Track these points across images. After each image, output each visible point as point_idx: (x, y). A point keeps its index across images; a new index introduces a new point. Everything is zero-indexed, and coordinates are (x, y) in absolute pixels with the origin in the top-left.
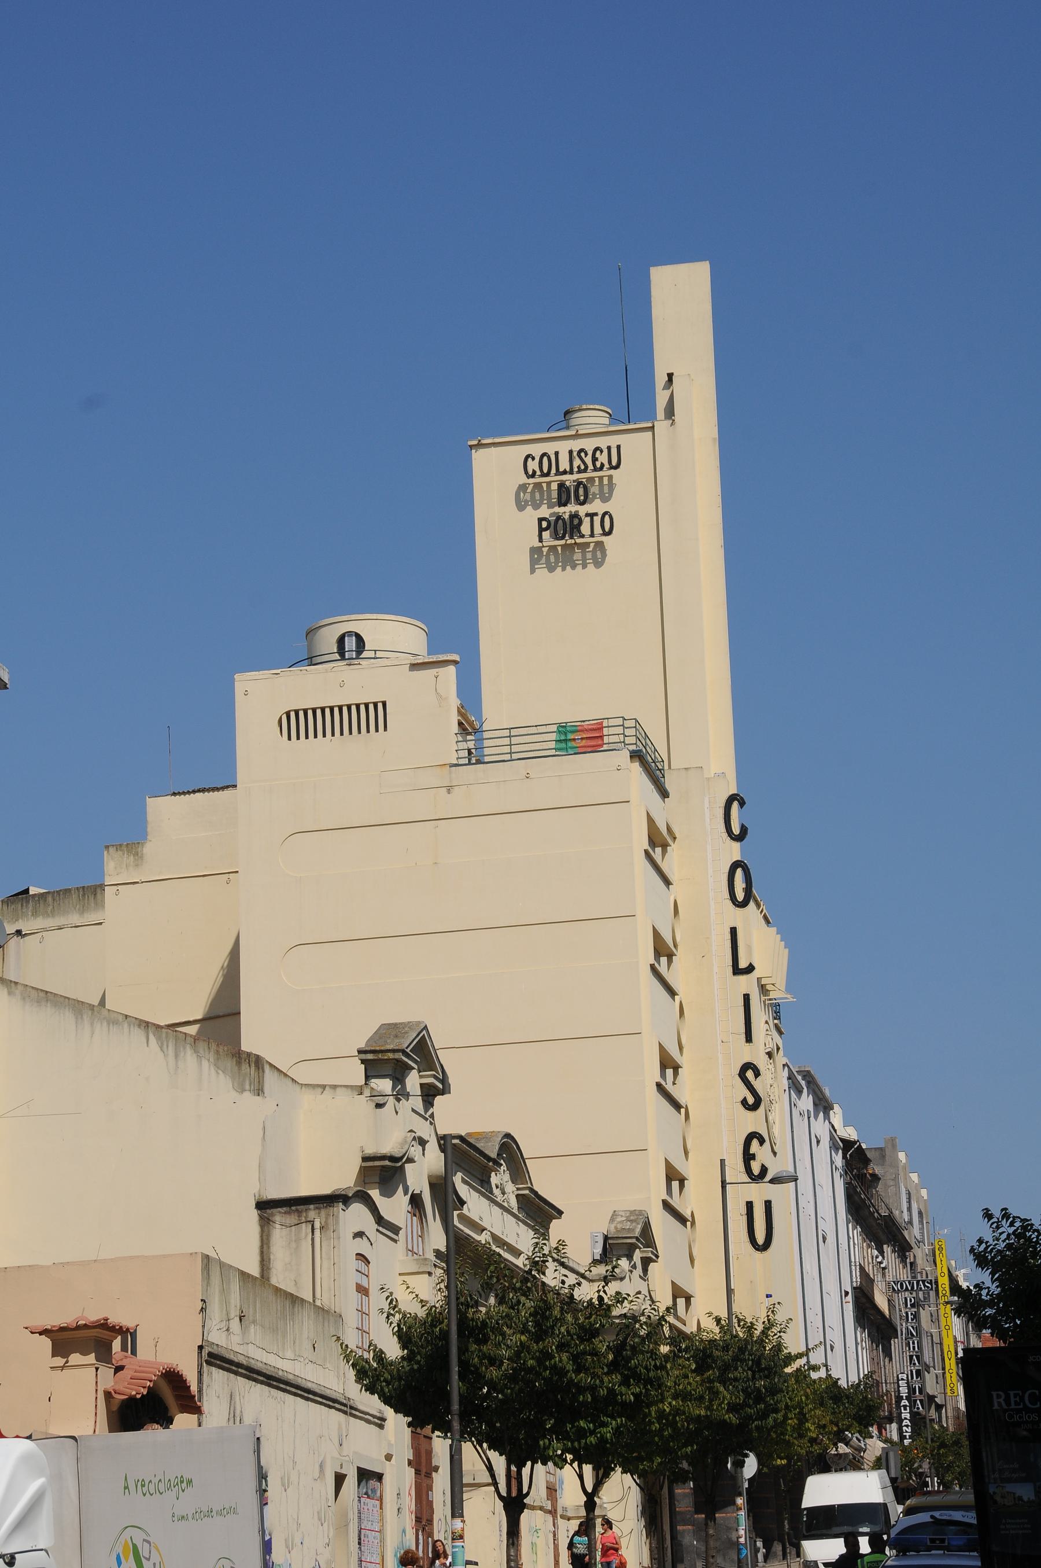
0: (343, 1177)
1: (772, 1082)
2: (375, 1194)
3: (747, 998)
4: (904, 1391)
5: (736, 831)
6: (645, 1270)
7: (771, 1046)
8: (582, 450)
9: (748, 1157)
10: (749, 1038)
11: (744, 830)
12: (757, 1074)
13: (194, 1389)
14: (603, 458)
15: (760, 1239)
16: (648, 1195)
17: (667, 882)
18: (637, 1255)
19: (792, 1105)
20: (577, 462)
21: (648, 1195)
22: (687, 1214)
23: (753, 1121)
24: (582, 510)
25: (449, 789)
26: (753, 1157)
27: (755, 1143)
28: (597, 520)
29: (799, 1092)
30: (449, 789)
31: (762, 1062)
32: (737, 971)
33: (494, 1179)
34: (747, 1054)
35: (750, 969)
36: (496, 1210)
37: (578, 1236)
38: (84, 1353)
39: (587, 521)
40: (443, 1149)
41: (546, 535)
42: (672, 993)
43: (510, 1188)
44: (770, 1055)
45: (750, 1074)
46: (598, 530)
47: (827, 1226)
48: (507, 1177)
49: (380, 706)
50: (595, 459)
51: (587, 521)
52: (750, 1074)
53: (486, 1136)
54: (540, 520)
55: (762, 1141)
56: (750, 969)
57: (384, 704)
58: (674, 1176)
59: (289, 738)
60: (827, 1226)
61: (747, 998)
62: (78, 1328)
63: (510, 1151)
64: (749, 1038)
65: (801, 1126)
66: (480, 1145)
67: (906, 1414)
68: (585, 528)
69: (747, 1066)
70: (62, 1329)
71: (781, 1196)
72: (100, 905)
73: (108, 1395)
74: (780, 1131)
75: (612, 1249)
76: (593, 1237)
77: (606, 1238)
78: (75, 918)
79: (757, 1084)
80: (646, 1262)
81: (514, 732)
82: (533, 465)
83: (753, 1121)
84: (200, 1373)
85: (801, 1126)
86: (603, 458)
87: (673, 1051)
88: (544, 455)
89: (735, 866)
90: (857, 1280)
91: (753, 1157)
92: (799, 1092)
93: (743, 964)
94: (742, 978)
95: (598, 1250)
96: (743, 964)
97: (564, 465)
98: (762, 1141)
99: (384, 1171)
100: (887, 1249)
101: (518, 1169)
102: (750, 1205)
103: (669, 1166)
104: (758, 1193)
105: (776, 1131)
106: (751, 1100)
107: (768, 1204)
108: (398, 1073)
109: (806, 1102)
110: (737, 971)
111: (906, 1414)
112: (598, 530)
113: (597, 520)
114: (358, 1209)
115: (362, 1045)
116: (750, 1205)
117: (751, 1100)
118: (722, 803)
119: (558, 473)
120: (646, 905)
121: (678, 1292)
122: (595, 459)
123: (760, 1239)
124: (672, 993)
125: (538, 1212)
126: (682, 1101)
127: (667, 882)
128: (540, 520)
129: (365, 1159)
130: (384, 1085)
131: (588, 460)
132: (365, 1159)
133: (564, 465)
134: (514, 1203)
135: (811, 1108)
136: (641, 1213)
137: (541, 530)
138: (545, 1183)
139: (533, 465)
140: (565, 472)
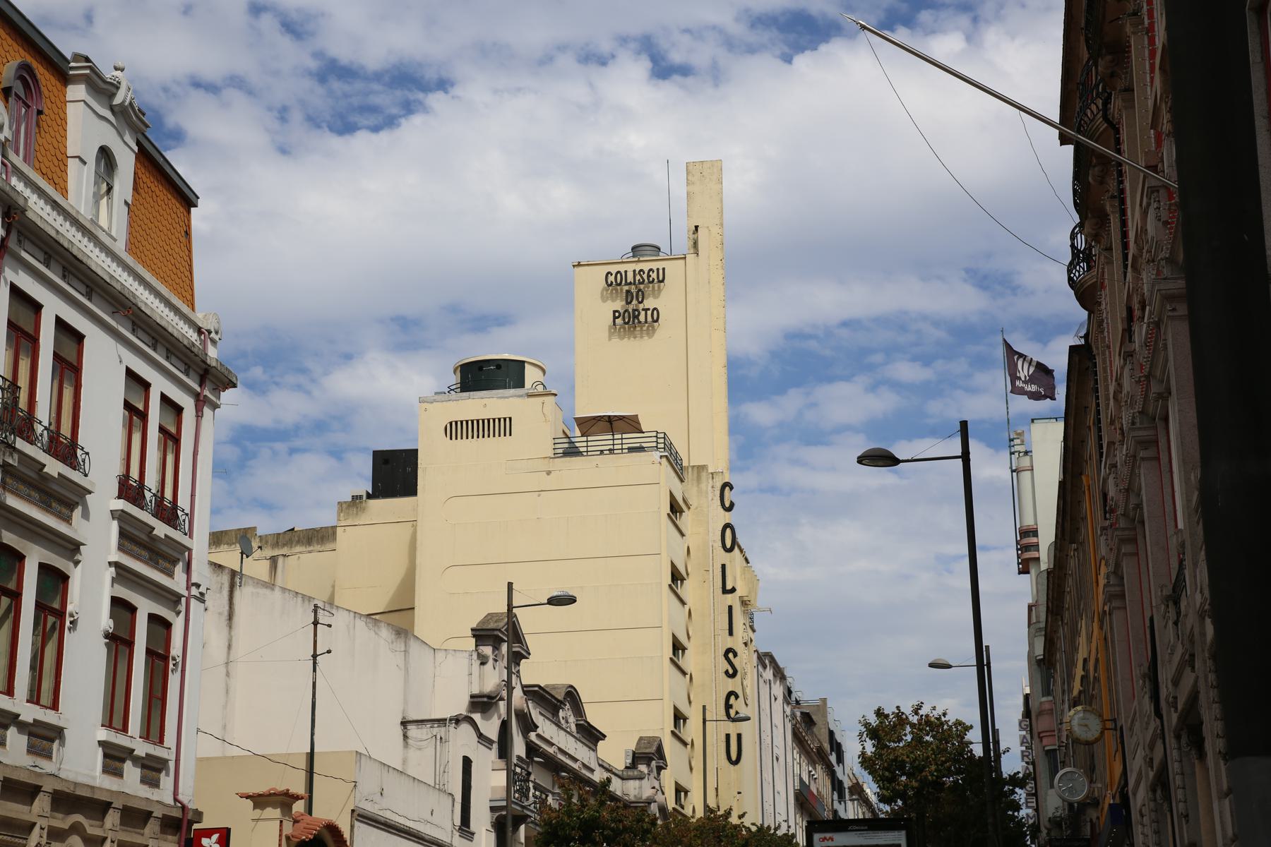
0: (460, 706)
1: (746, 660)
2: (477, 717)
3: (730, 608)
5: (727, 505)
6: (659, 774)
7: (746, 639)
9: (728, 707)
10: (731, 633)
11: (732, 505)
12: (735, 655)
13: (347, 835)
14: (654, 275)
15: (734, 757)
16: (661, 727)
17: (682, 535)
18: (654, 763)
19: (759, 675)
20: (638, 277)
21: (661, 727)
22: (689, 741)
23: (732, 685)
25: (549, 473)
26: (731, 706)
27: (733, 698)
28: (649, 313)
29: (765, 667)
30: (549, 473)
31: (740, 648)
32: (725, 591)
33: (561, 714)
34: (729, 643)
35: (733, 590)
36: (562, 733)
37: (615, 752)
38: (275, 808)
39: (643, 313)
40: (525, 693)
42: (683, 603)
43: (572, 719)
44: (746, 644)
45: (731, 655)
46: (649, 319)
47: (779, 751)
48: (570, 713)
50: (649, 276)
51: (643, 313)
52: (731, 655)
53: (554, 687)
54: (615, 312)
55: (737, 697)
56: (733, 590)
58: (679, 717)
60: (779, 751)
61: (730, 608)
62: (270, 795)
63: (572, 696)
64: (731, 633)
65: (765, 690)
66: (553, 693)
68: (642, 318)
69: (729, 650)
70: (260, 795)
71: (743, 727)
72: (334, 539)
73: (288, 838)
74: (751, 691)
75: (638, 758)
76: (627, 752)
77: (634, 753)
78: (318, 547)
79: (736, 662)
80: (659, 769)
82: (611, 278)
83: (732, 685)
84: (352, 827)
85: (765, 690)
86: (654, 275)
87: (682, 638)
89: (727, 526)
91: (731, 706)
92: (765, 667)
93: (729, 587)
94: (729, 596)
95: (629, 761)
96: (729, 587)
97: (630, 279)
99: (483, 703)
100: (819, 767)
101: (578, 708)
102: (728, 736)
103: (676, 710)
104: (732, 728)
105: (748, 691)
106: (731, 671)
107: (739, 736)
108: (496, 642)
109: (769, 674)
110: (725, 591)
112: (649, 319)
113: (649, 313)
114: (465, 728)
115: (474, 626)
116: (728, 736)
117: (731, 671)
119: (627, 284)
120: (669, 547)
121: (680, 790)
122: (649, 276)
123: (734, 757)
124: (683, 603)
125: (591, 736)
126: (688, 670)
127: (682, 535)
128: (615, 312)
129: (472, 697)
130: (487, 650)
131: (645, 276)
132: (472, 697)
133: (630, 279)
134: (574, 728)
135: (771, 678)
136: (654, 738)
137: (615, 318)
138: (594, 717)
139: (611, 278)
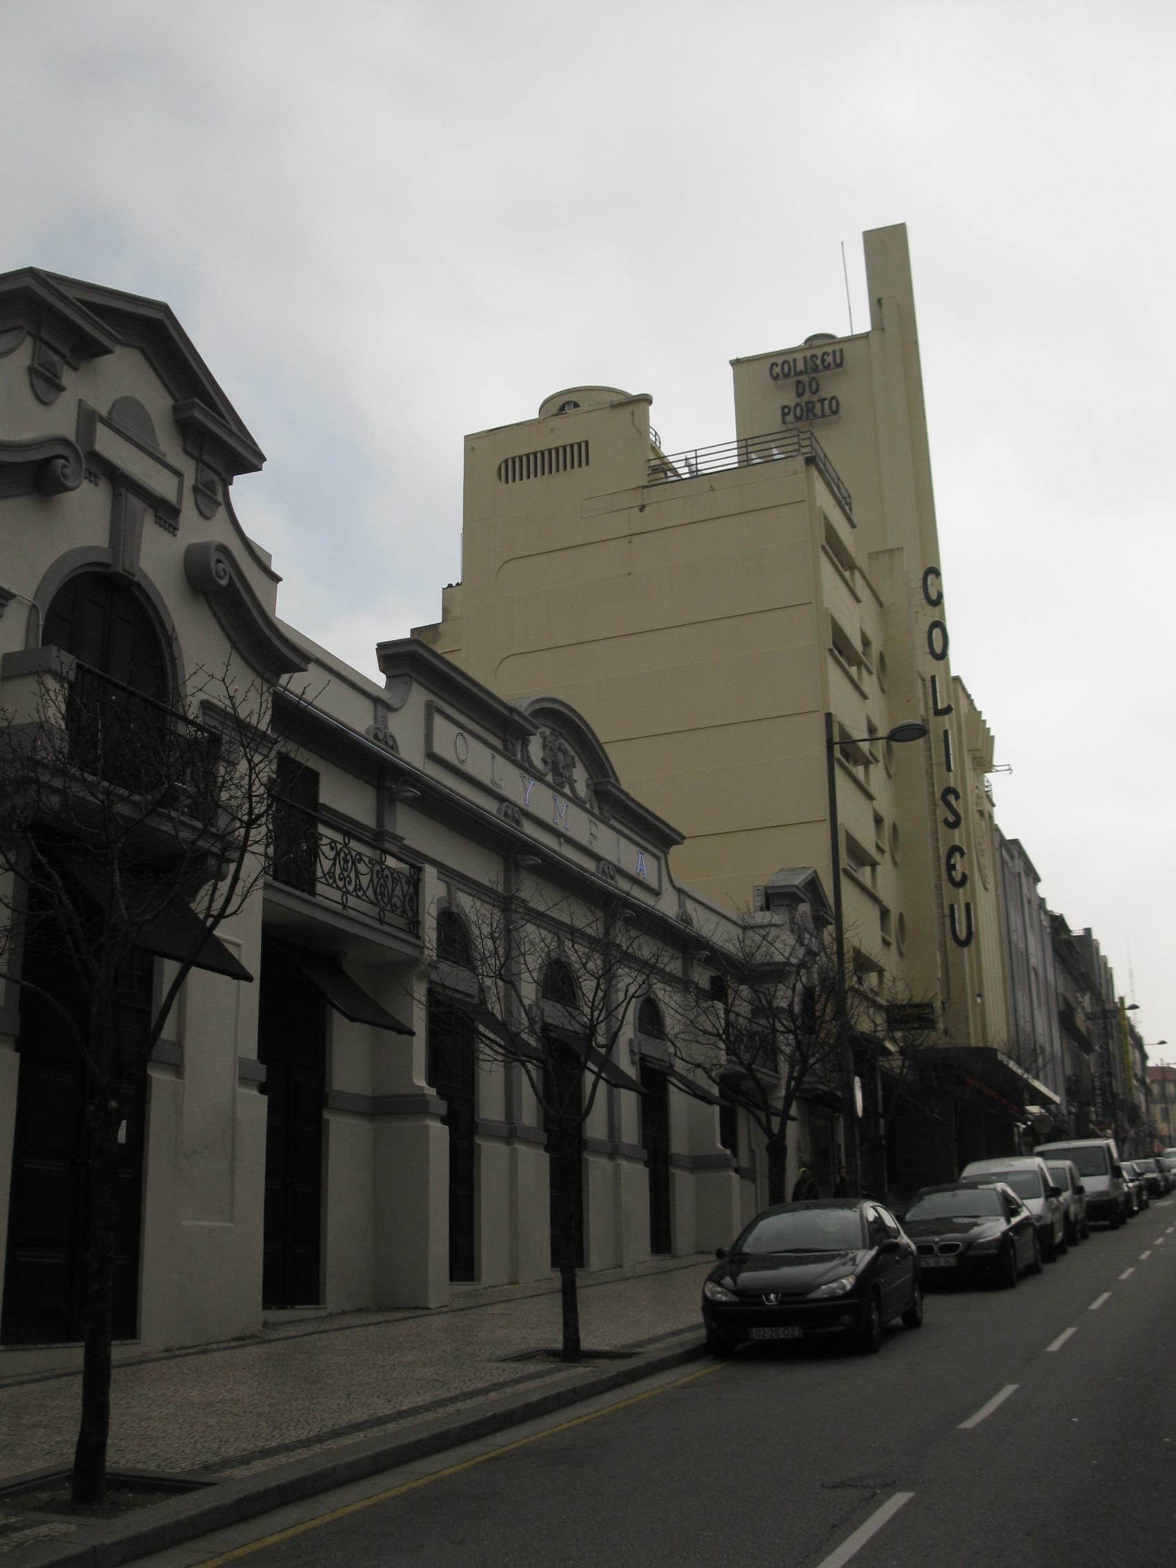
4: (1097, 1084)
8: (813, 356)
24: (815, 398)
25: (642, 508)
28: (826, 404)
35: (948, 710)
39: (818, 405)
41: (790, 418)
49: (583, 446)
50: (823, 361)
51: (818, 405)
55: (962, 853)
56: (948, 710)
57: (587, 443)
59: (507, 482)
67: (1099, 1100)
81: (699, 453)
82: (777, 370)
86: (829, 359)
88: (785, 362)
90: (1062, 1007)
98: (962, 853)
110: (939, 713)
111: (1099, 1100)
112: (827, 411)
113: (826, 404)
118: (921, 575)
122: (823, 361)
128: (783, 408)
131: (819, 362)
137: (784, 415)
139: (777, 370)
140: (801, 372)
